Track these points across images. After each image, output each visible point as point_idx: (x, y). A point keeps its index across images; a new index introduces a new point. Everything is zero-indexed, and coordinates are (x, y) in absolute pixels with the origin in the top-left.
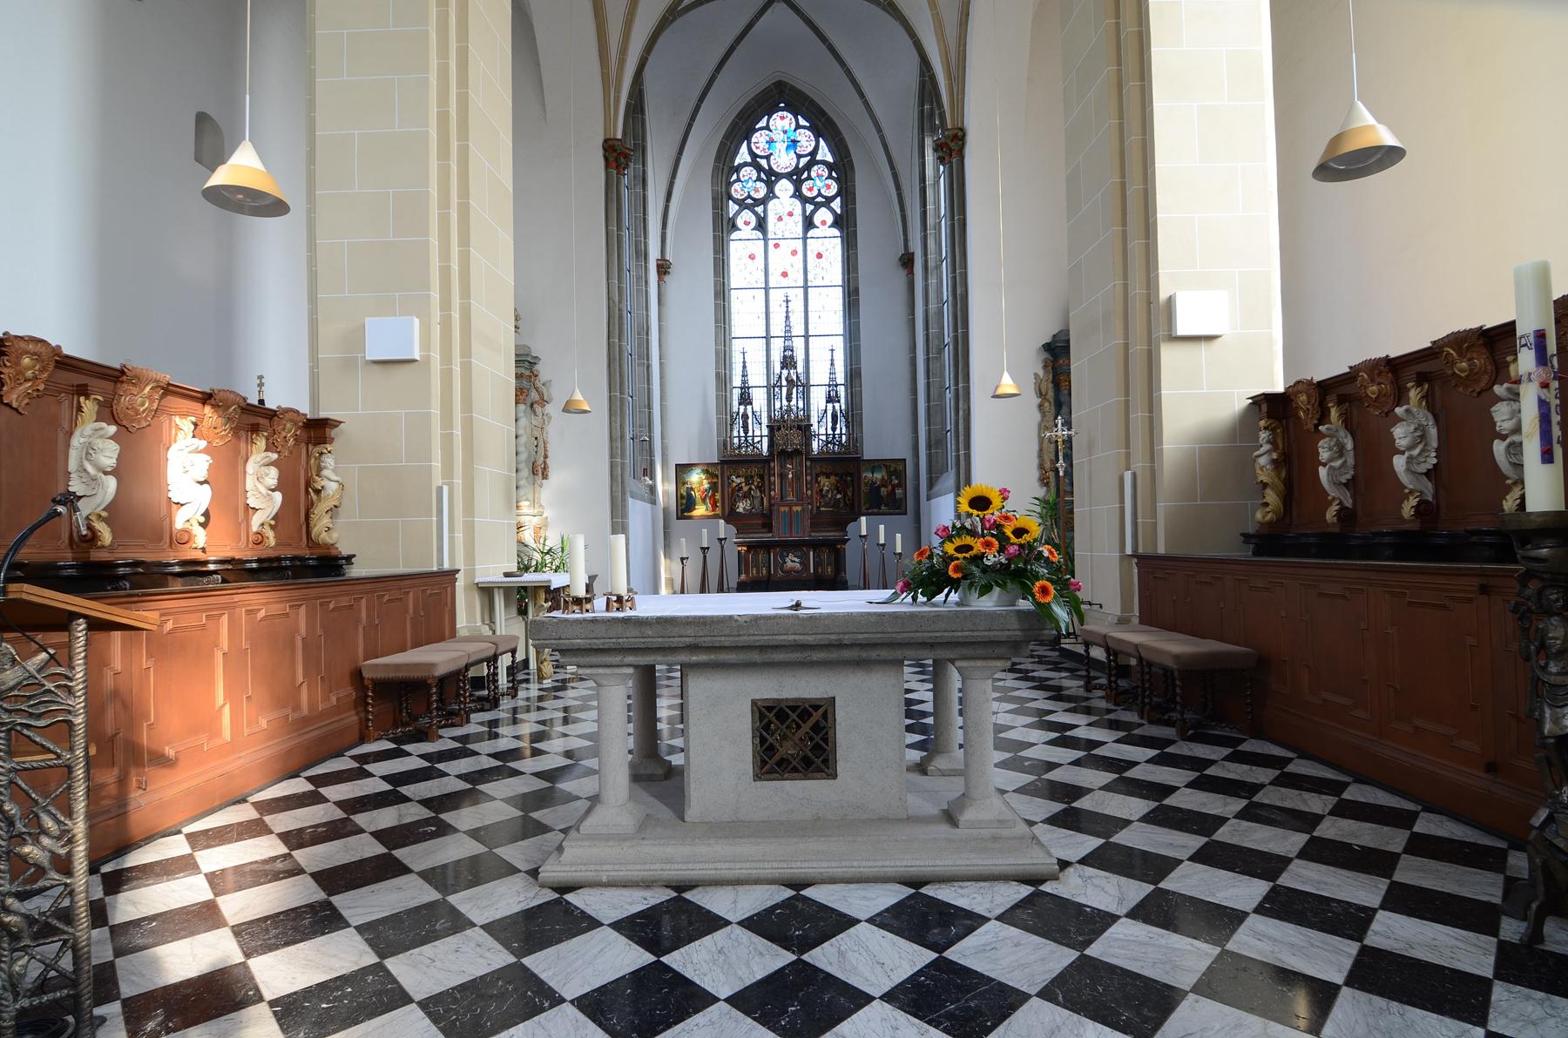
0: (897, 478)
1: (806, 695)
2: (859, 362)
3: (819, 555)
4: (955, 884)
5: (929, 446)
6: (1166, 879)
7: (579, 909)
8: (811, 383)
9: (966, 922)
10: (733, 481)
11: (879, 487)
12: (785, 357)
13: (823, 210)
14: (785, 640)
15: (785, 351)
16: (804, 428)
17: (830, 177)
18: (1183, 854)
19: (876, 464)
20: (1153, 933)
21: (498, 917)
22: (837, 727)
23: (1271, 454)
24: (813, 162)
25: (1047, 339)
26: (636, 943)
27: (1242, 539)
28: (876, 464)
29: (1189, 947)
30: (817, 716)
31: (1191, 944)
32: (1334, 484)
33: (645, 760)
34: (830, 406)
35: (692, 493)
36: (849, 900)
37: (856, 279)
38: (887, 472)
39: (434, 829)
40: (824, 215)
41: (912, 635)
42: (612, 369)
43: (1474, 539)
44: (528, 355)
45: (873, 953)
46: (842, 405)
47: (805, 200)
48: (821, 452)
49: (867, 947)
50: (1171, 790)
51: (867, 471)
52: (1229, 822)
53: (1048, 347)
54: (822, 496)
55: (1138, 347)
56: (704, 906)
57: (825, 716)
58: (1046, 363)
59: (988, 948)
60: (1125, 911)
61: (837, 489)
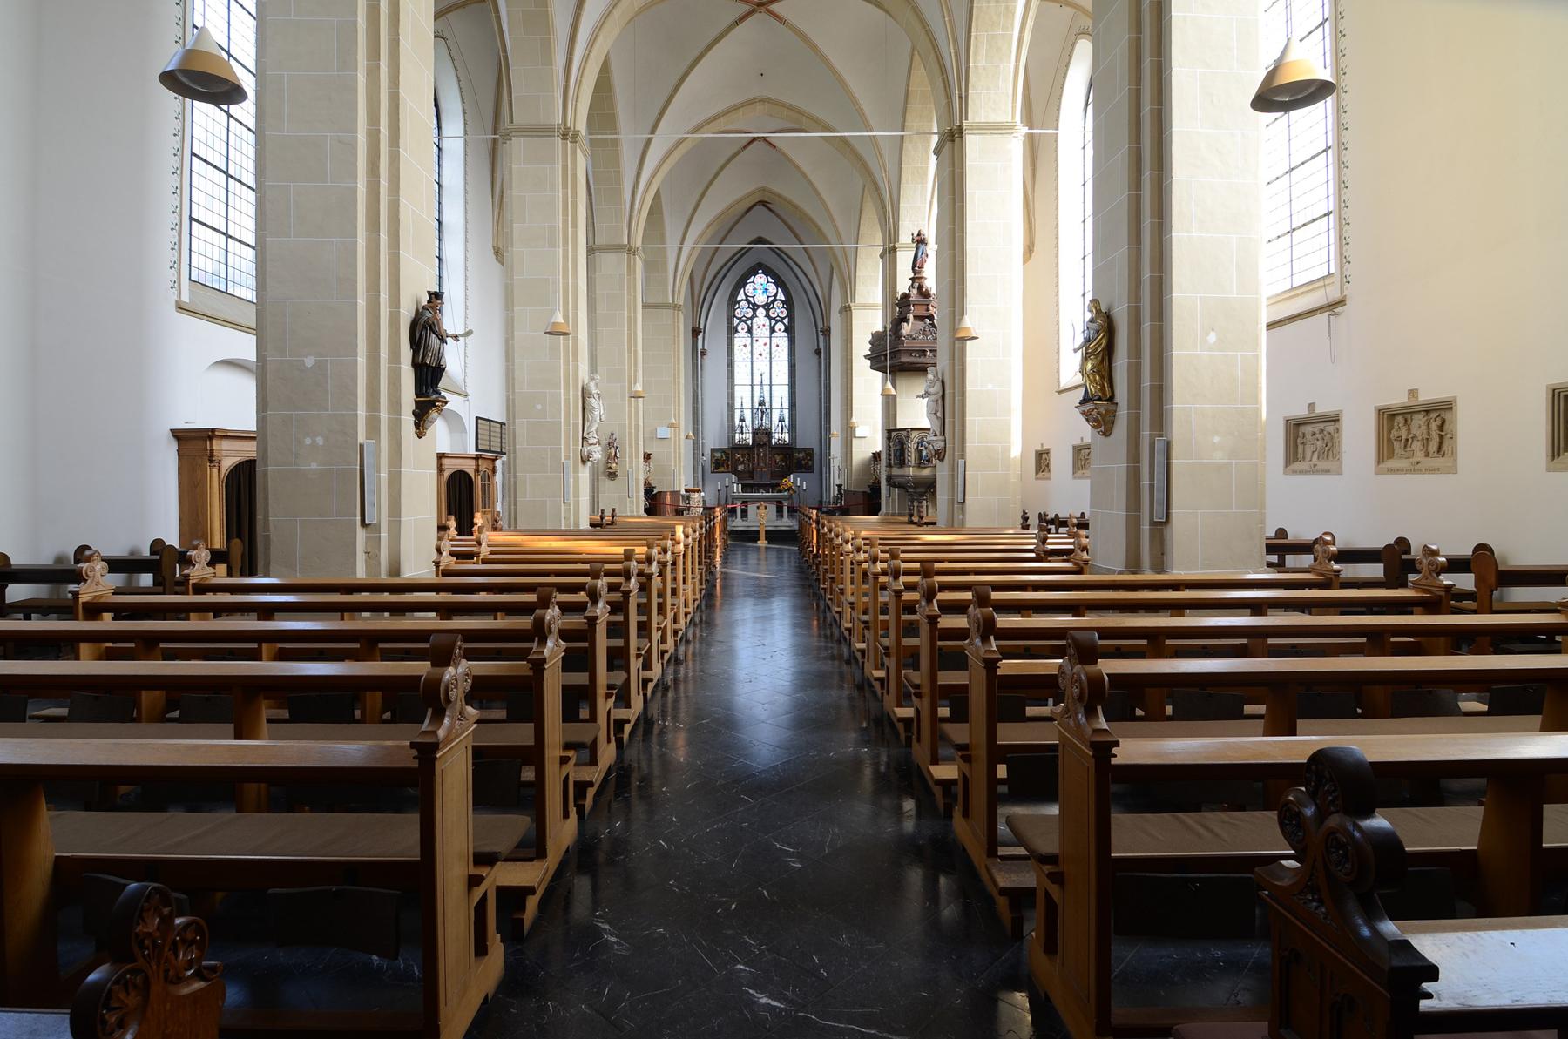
16: (769, 434)
17: (783, 307)
40: (780, 326)
47: (771, 319)
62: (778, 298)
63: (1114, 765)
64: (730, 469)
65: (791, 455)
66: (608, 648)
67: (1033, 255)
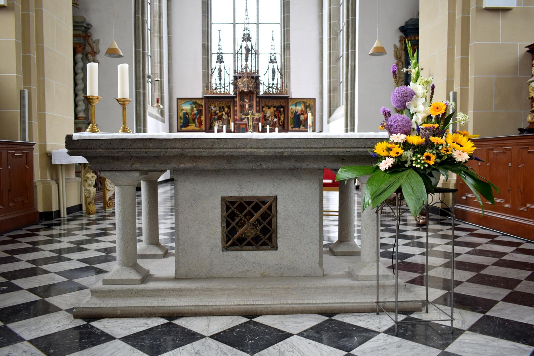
1: (258, 194)
4: (355, 314)
5: (330, 92)
6: (490, 311)
7: (99, 330)
9: (364, 334)
10: (212, 109)
12: (244, 35)
14: (244, 152)
15: (244, 30)
16: (255, 79)
18: (499, 298)
20: (487, 339)
21: (42, 335)
22: (278, 215)
25: (403, 24)
26: (138, 349)
29: (513, 347)
30: (264, 208)
31: (514, 345)
33: (150, 245)
34: (271, 64)
35: (187, 116)
36: (285, 323)
38: (304, 106)
39: (5, 288)
41: (330, 150)
42: (137, 33)
44: (83, 22)
45: (302, 352)
46: (278, 65)
48: (265, 93)
49: (299, 349)
50: (484, 267)
52: (523, 282)
53: (402, 29)
56: (186, 327)
57: (270, 208)
58: (401, 38)
59: (380, 349)
60: (467, 328)
64: (203, 127)
66: (360, 255)
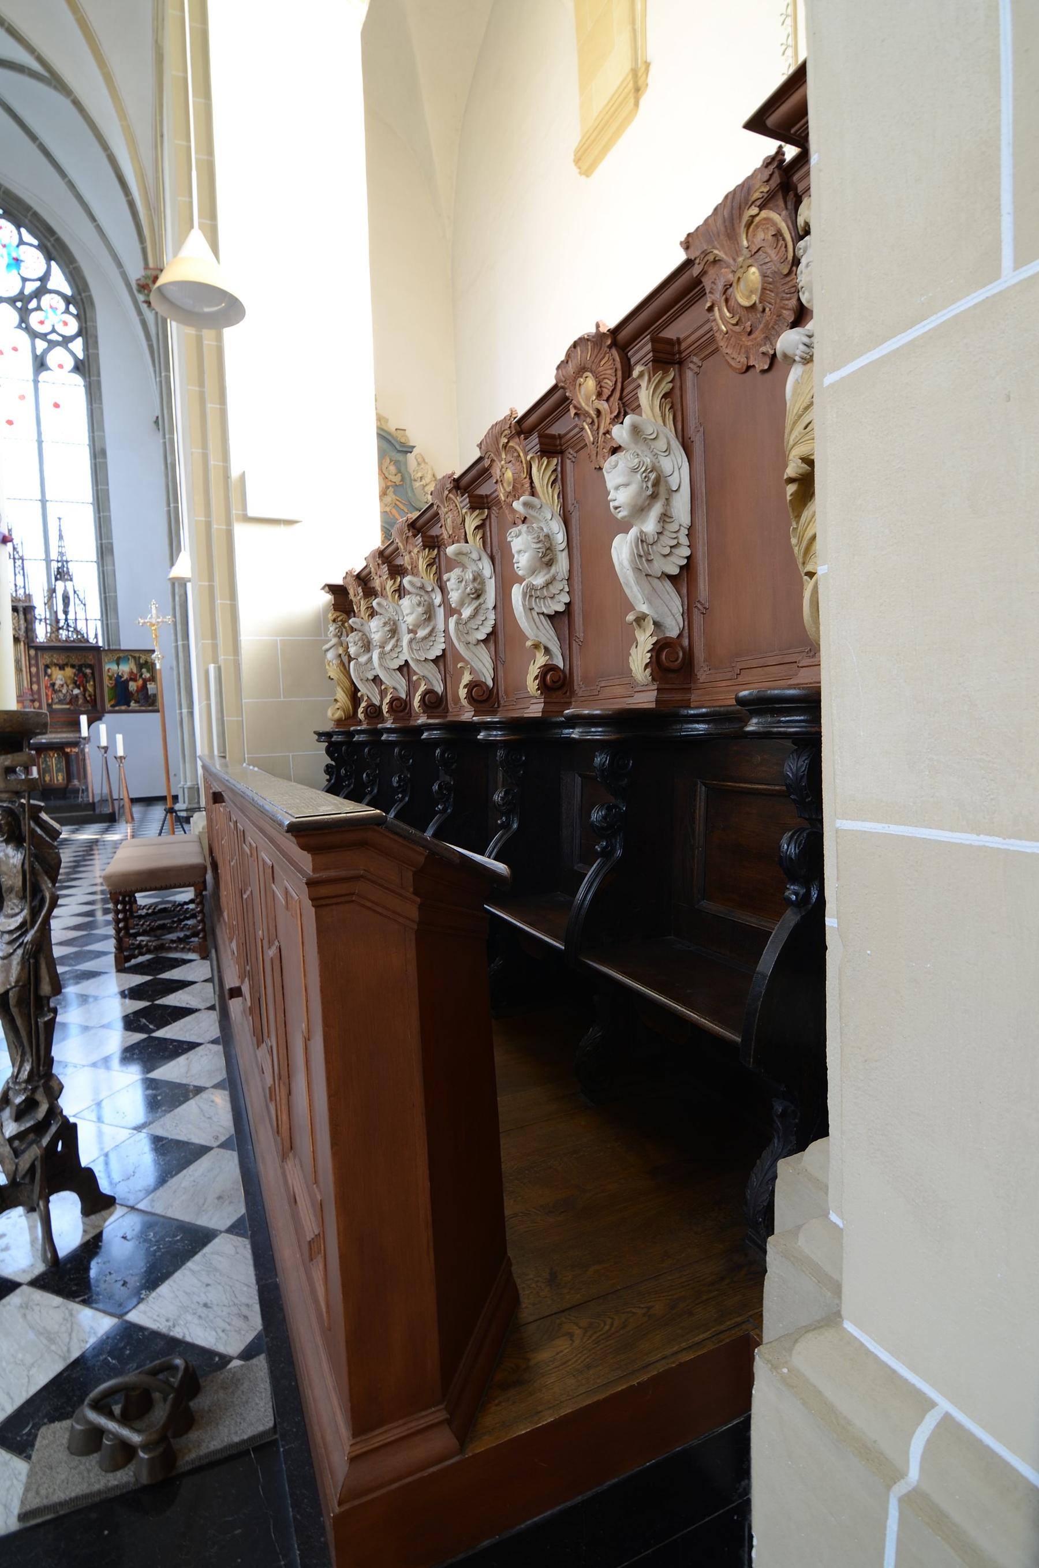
0: (148, 671)
2: (109, 535)
3: (46, 761)
8: (52, 559)
11: (126, 682)
13: (59, 350)
17: (67, 311)
19: (121, 655)
23: (337, 649)
24: (41, 291)
27: (316, 737)
28: (121, 655)
32: (361, 680)
37: (103, 438)
38: (136, 664)
40: (58, 357)
43: (753, 725)
47: (34, 335)
51: (109, 662)
54: (55, 691)
55: (218, 526)
61: (75, 683)
62: (50, 286)
63: (79, 718)
65: (96, 669)
67: (644, 101)
